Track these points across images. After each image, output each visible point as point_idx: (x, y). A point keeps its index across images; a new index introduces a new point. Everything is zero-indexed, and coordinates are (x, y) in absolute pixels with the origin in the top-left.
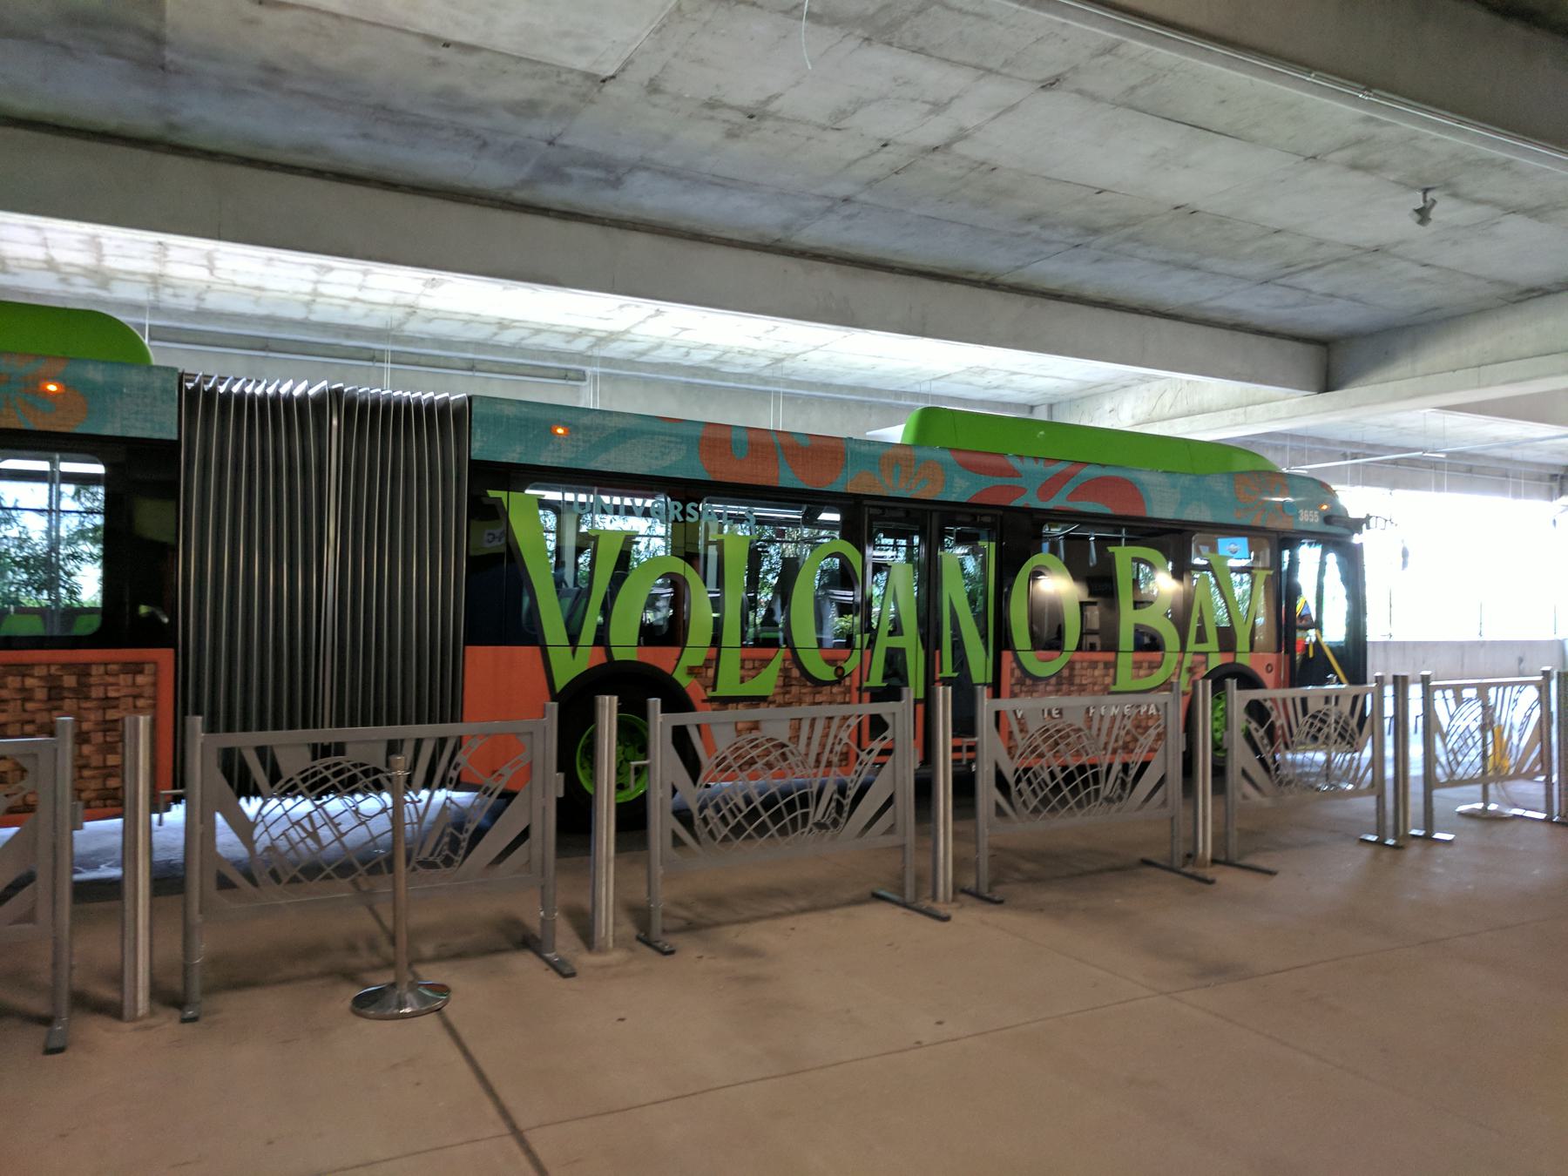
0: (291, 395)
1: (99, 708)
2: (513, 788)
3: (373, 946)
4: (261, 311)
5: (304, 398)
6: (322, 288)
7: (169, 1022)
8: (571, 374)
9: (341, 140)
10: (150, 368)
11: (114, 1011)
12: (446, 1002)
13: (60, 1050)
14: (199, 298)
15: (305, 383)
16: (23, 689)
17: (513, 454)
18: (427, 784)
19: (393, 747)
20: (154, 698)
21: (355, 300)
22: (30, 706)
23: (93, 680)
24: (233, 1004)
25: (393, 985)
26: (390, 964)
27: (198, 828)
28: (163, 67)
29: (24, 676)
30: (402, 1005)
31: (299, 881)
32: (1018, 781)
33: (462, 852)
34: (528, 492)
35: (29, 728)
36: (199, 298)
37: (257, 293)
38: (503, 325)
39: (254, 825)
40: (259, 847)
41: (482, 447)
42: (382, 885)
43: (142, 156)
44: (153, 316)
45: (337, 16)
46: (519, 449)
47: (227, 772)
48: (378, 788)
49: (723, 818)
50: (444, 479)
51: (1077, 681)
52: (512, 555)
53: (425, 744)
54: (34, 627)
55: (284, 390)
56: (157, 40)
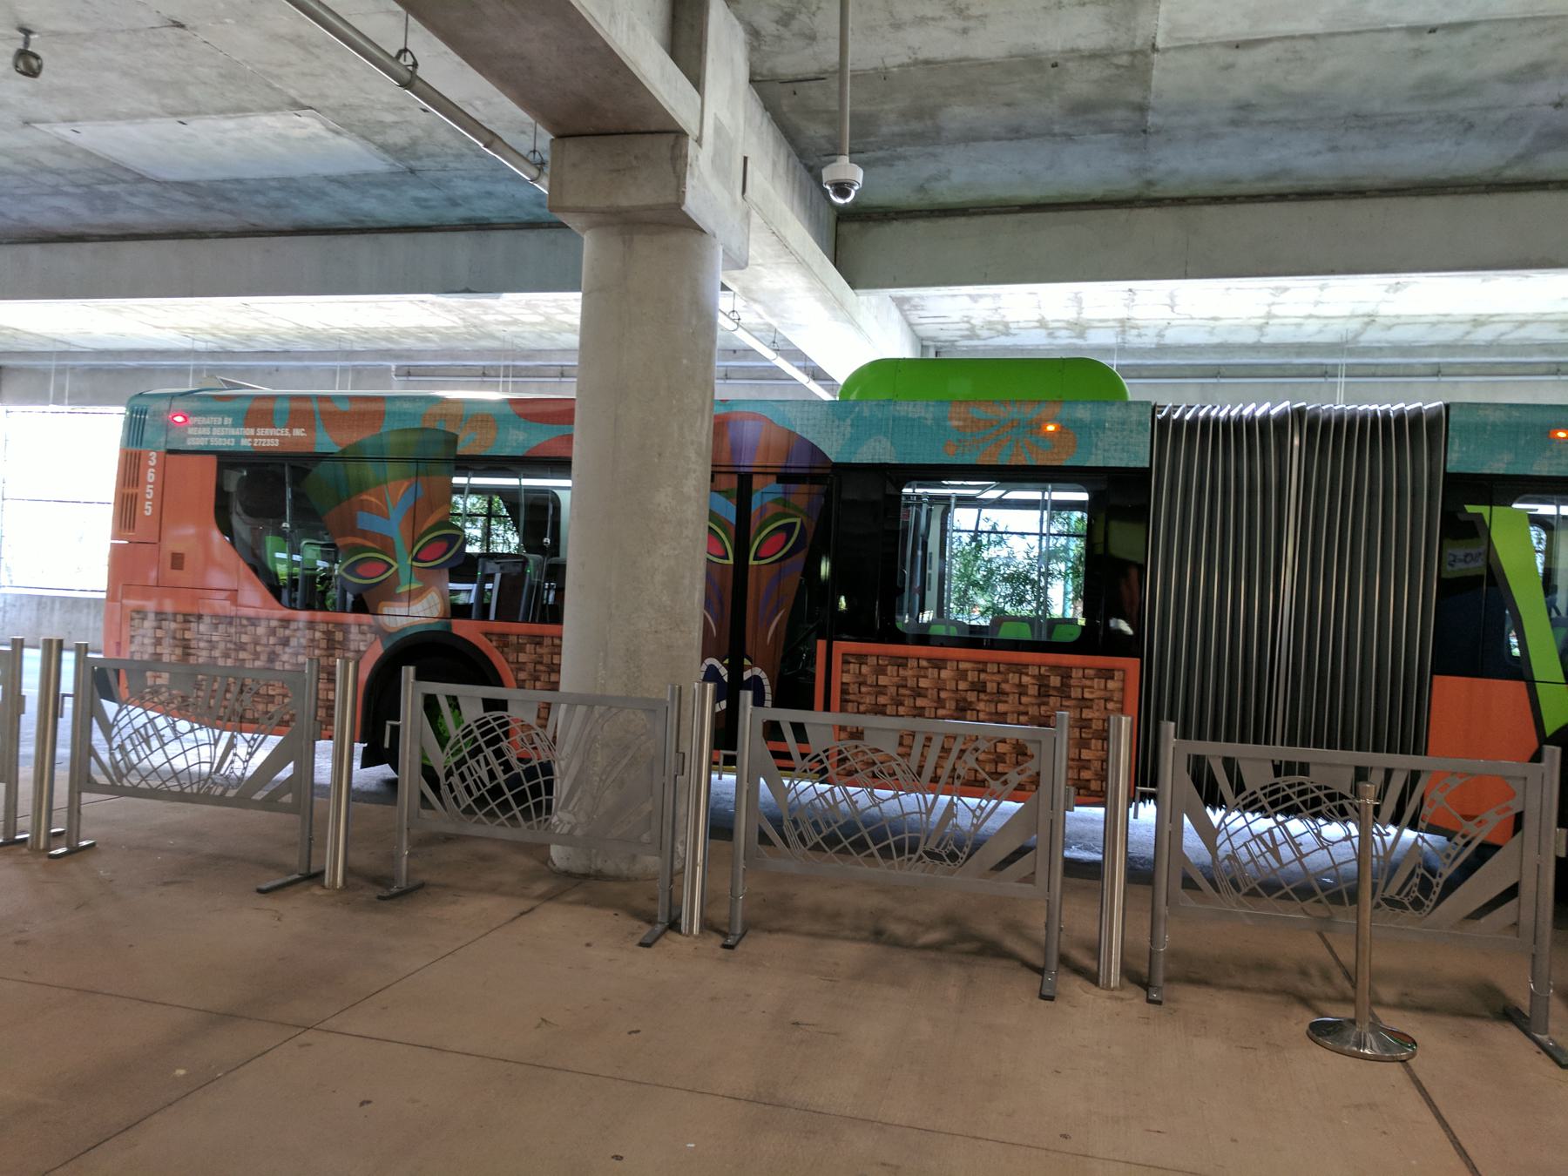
0: (1254, 418)
1: (1076, 707)
2: (1497, 842)
3: (1326, 977)
4: (1215, 340)
5: (1265, 419)
6: (1276, 310)
7: (1135, 997)
8: (1223, 370)
9: (1307, 159)
10: (1128, 404)
11: (1093, 978)
12: (1413, 1055)
13: (1051, 999)
14: (1160, 335)
15: (1268, 405)
16: (1020, 685)
17: (1499, 464)
18: (1396, 821)
19: (1361, 774)
20: (1122, 702)
21: (1310, 316)
22: (1024, 700)
23: (1073, 682)
24: (1192, 998)
25: (1353, 1022)
26: (1345, 999)
27: (1167, 827)
28: (1145, 131)
29: (940, 669)
30: (1361, 1043)
31: (1259, 896)
32: (449, 774)
33: (1434, 897)
34: (1516, 506)
35: (1023, 718)
36: (1160, 335)
37: (1212, 323)
38: (1477, 322)
39: (1217, 831)
40: (1221, 853)
41: (1461, 458)
42: (1343, 916)
43: (1122, 215)
44: (1120, 357)
45: (1313, 37)
46: (1507, 457)
47: (1197, 780)
48: (1342, 815)
49: (468, 788)
50: (1413, 496)
51: (1076, 693)
52: (1492, 581)
53: (1395, 775)
54: (1025, 633)
55: (1245, 413)
56: (1142, 108)
